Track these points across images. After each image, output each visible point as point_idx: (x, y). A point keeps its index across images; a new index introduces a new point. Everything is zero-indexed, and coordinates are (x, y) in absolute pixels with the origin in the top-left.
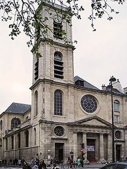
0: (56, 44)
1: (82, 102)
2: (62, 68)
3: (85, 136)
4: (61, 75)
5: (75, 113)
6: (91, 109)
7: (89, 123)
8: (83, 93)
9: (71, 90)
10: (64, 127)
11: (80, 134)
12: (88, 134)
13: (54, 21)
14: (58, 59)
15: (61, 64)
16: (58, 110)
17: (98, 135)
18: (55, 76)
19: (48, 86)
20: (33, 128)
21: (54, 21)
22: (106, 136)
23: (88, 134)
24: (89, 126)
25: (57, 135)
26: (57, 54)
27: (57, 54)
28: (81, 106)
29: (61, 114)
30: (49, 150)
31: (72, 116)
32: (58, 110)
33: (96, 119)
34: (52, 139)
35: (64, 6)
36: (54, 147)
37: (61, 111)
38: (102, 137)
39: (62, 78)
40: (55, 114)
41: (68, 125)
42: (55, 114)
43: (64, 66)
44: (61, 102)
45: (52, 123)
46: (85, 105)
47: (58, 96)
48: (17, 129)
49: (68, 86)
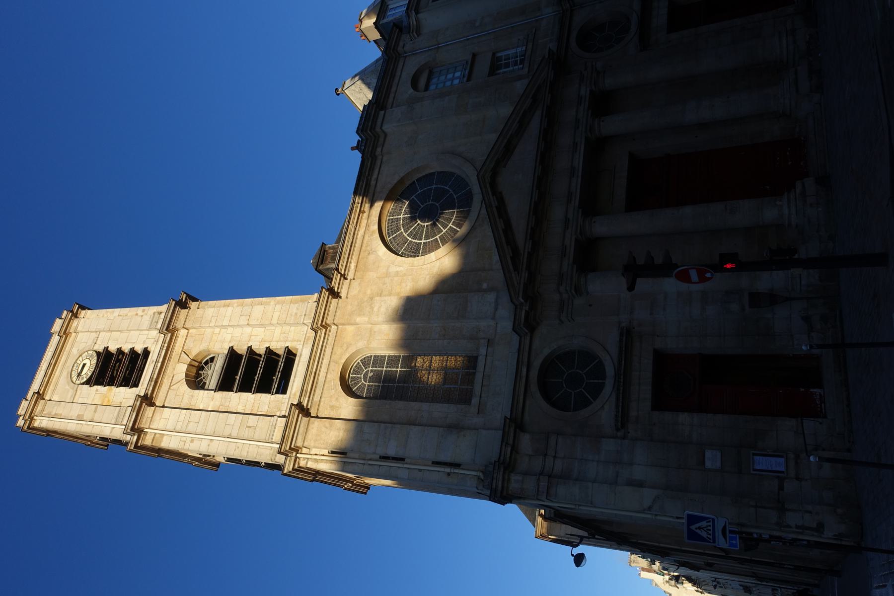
3: (601, 227)
7: (518, 207)
10: (549, 340)
11: (587, 256)
12: (590, 206)
13: (88, 382)
14: (213, 374)
15: (233, 356)
17: (597, 148)
22: (603, 103)
23: (590, 206)
24: (538, 212)
25: (596, 391)
33: (495, 173)
34: (622, 420)
36: (684, 418)
38: (612, 125)
45: (515, 424)
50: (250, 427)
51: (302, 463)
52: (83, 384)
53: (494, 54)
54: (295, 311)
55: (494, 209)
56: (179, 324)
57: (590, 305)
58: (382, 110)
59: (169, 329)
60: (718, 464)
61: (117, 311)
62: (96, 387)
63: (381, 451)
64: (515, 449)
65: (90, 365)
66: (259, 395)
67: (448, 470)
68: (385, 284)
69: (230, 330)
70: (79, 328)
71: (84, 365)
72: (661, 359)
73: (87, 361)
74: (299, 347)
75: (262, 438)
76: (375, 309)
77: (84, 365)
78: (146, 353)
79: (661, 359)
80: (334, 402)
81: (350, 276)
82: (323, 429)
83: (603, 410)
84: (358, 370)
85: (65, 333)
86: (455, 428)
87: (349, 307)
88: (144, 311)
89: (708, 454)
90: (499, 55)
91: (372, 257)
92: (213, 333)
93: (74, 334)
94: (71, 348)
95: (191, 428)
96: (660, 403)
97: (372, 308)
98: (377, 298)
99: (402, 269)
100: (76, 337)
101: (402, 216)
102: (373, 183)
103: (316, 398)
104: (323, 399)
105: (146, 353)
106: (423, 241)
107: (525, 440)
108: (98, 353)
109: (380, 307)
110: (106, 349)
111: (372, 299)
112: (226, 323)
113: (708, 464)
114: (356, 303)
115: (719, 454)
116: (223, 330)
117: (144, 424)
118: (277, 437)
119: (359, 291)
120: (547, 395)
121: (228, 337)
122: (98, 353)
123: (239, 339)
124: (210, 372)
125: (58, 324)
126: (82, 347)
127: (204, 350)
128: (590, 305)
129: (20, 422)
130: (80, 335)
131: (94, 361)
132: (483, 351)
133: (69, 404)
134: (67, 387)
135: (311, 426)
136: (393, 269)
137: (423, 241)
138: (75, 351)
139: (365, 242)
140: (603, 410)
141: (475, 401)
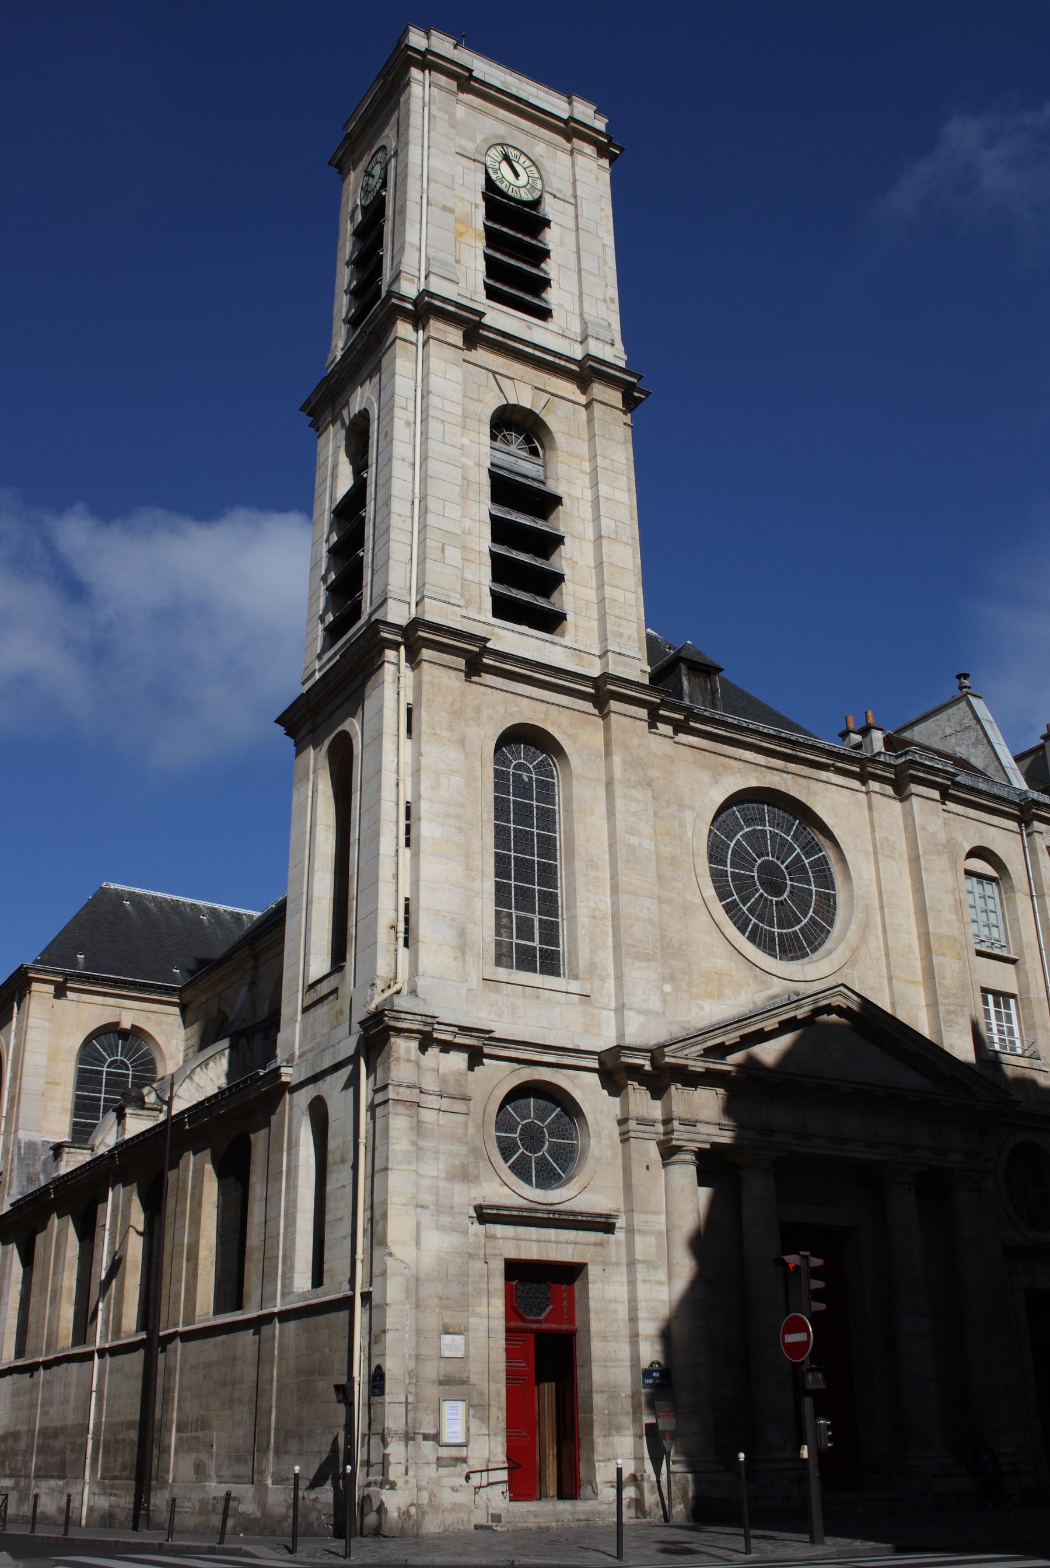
0: (506, 346)
1: (716, 854)
2: (550, 543)
4: (541, 602)
5: (670, 953)
6: (786, 921)
8: (716, 777)
9: (628, 720)
10: (585, 1089)
13: (490, 185)
14: (521, 464)
15: (546, 503)
16: (530, 922)
18: (503, 608)
19: (441, 676)
20: (303, 1098)
21: (490, 185)
25: (521, 1170)
26: (515, 424)
27: (515, 424)
28: (710, 892)
29: (550, 965)
30: (452, 1345)
31: (644, 983)
32: (530, 922)
34: (485, 1215)
35: (406, 1167)
37: (550, 933)
39: (550, 622)
40: (501, 959)
41: (614, 1071)
42: (501, 959)
43: (562, 522)
44: (548, 846)
46: (744, 886)
47: (523, 789)
48: (136, 1125)
49: (602, 693)
50: (443, 551)
51: (390, 654)
52: (487, 173)
53: (1014, 996)
54: (626, 632)
55: (791, 1014)
56: (598, 390)
57: (648, 1167)
58: (941, 794)
59: (586, 373)
60: (447, 1354)
61: (609, 240)
62: (482, 204)
63: (425, 808)
64: (447, 1047)
65: (518, 185)
66: (489, 562)
67: (401, 927)
68: (668, 803)
69: (588, 495)
70: (579, 159)
71: (517, 175)
72: (569, 1274)
73: (523, 180)
74: (567, 640)
75: (430, 578)
76: (634, 792)
77: (517, 175)
78: (543, 314)
79: (569, 1274)
80: (486, 712)
81: (682, 737)
82: (449, 698)
83: (505, 1189)
84: (544, 769)
85: (570, 130)
86: (463, 946)
87: (635, 741)
88: (612, 300)
89: (459, 1339)
90: (1012, 1001)
91: (705, 776)
92: (583, 459)
93: (568, 146)
94: (548, 143)
95: (434, 426)
96: (518, 1271)
97: (634, 786)
98: (650, 795)
99: (690, 834)
100: (563, 150)
101: (768, 828)
102: (824, 775)
103: (488, 679)
104: (489, 690)
105: (543, 314)
106: (729, 869)
107: (458, 1060)
108: (536, 203)
109: (637, 801)
110: (547, 223)
111: (649, 784)
112: (603, 489)
113: (446, 1339)
114: (642, 755)
115: (67, 1149)
116: (587, 479)
117: (436, 327)
118: (434, 613)
119: (655, 755)
120: (516, 1094)
121: (576, 492)
122: (536, 203)
123: (575, 513)
124: (513, 448)
125: (584, 111)
126: (546, 163)
127: (552, 439)
128: (648, 1167)
129: (416, 39)
130: (566, 158)
131: (526, 196)
132: (574, 986)
133: (452, 150)
134: (479, 138)
135: (453, 673)
136: (689, 816)
137: (729, 869)
138: (539, 150)
139: (731, 761)
140: (505, 1189)
141: (502, 973)
